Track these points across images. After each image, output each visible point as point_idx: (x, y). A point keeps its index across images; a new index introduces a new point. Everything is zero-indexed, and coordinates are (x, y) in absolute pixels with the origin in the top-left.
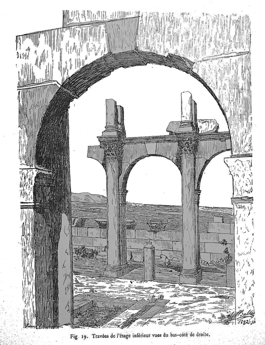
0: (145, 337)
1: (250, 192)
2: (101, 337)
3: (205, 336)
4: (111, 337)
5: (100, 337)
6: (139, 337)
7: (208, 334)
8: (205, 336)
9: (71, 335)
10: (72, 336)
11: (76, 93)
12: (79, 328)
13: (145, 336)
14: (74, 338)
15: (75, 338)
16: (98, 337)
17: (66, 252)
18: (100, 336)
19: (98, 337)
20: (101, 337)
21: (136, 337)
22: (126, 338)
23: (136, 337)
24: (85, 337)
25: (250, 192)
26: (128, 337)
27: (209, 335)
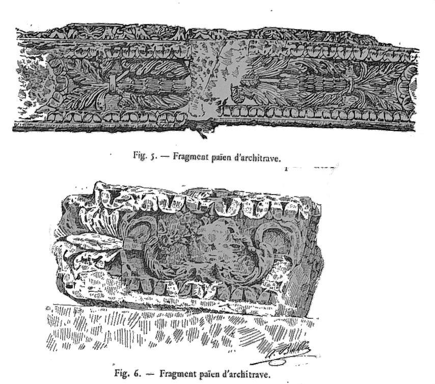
0: (213, 377)
1: (52, 334)
2: (262, 376)
3: (261, 161)
4: (224, 377)
5: (259, 375)
6: (239, 377)
7: (277, 159)
8: (260, 161)
9: (116, 370)
10: (118, 373)
11: (118, 256)
12: (250, 30)
13: (267, 159)
14: (121, 375)
15: (141, 158)
16: (267, 161)
17: (204, 112)
18: (260, 374)
19: (169, 376)
20: (262, 376)
21: (244, 377)
22: (173, 378)
23: (192, 376)
24: (136, 375)
25: (52, 334)
26: (176, 375)
27: (268, 376)
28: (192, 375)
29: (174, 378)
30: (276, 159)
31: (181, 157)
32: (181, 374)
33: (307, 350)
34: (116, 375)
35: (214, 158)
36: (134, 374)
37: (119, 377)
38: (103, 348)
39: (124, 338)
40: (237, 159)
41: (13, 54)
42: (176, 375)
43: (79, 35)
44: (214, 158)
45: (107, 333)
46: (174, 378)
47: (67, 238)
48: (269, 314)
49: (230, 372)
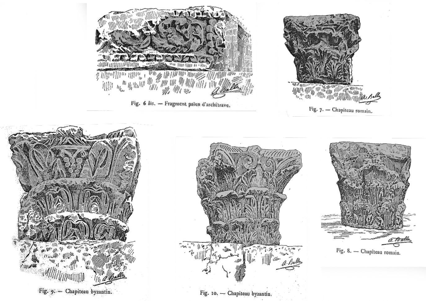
26: (175, 104)
28: (185, 104)
29: (174, 106)
30: (227, 106)
31: (170, 104)
32: (178, 104)
33: (379, 98)
34: (201, 294)
35: (190, 105)
36: (225, 96)
37: (42, 293)
38: (112, 89)
39: (320, 95)
40: (203, 105)
41: (355, 12)
42: (175, 104)
43: (380, 211)
44: (190, 105)
45: (211, 83)
46: (174, 106)
47: (238, 85)
48: (157, 105)
49: (206, 103)
